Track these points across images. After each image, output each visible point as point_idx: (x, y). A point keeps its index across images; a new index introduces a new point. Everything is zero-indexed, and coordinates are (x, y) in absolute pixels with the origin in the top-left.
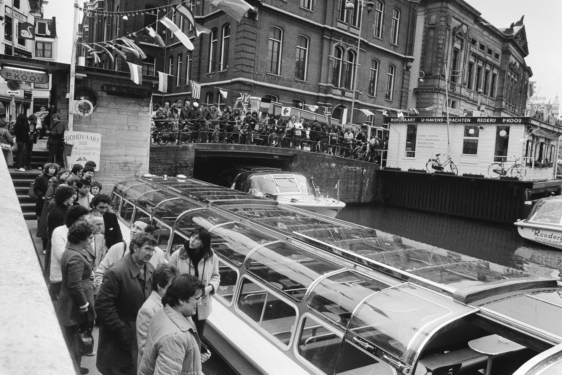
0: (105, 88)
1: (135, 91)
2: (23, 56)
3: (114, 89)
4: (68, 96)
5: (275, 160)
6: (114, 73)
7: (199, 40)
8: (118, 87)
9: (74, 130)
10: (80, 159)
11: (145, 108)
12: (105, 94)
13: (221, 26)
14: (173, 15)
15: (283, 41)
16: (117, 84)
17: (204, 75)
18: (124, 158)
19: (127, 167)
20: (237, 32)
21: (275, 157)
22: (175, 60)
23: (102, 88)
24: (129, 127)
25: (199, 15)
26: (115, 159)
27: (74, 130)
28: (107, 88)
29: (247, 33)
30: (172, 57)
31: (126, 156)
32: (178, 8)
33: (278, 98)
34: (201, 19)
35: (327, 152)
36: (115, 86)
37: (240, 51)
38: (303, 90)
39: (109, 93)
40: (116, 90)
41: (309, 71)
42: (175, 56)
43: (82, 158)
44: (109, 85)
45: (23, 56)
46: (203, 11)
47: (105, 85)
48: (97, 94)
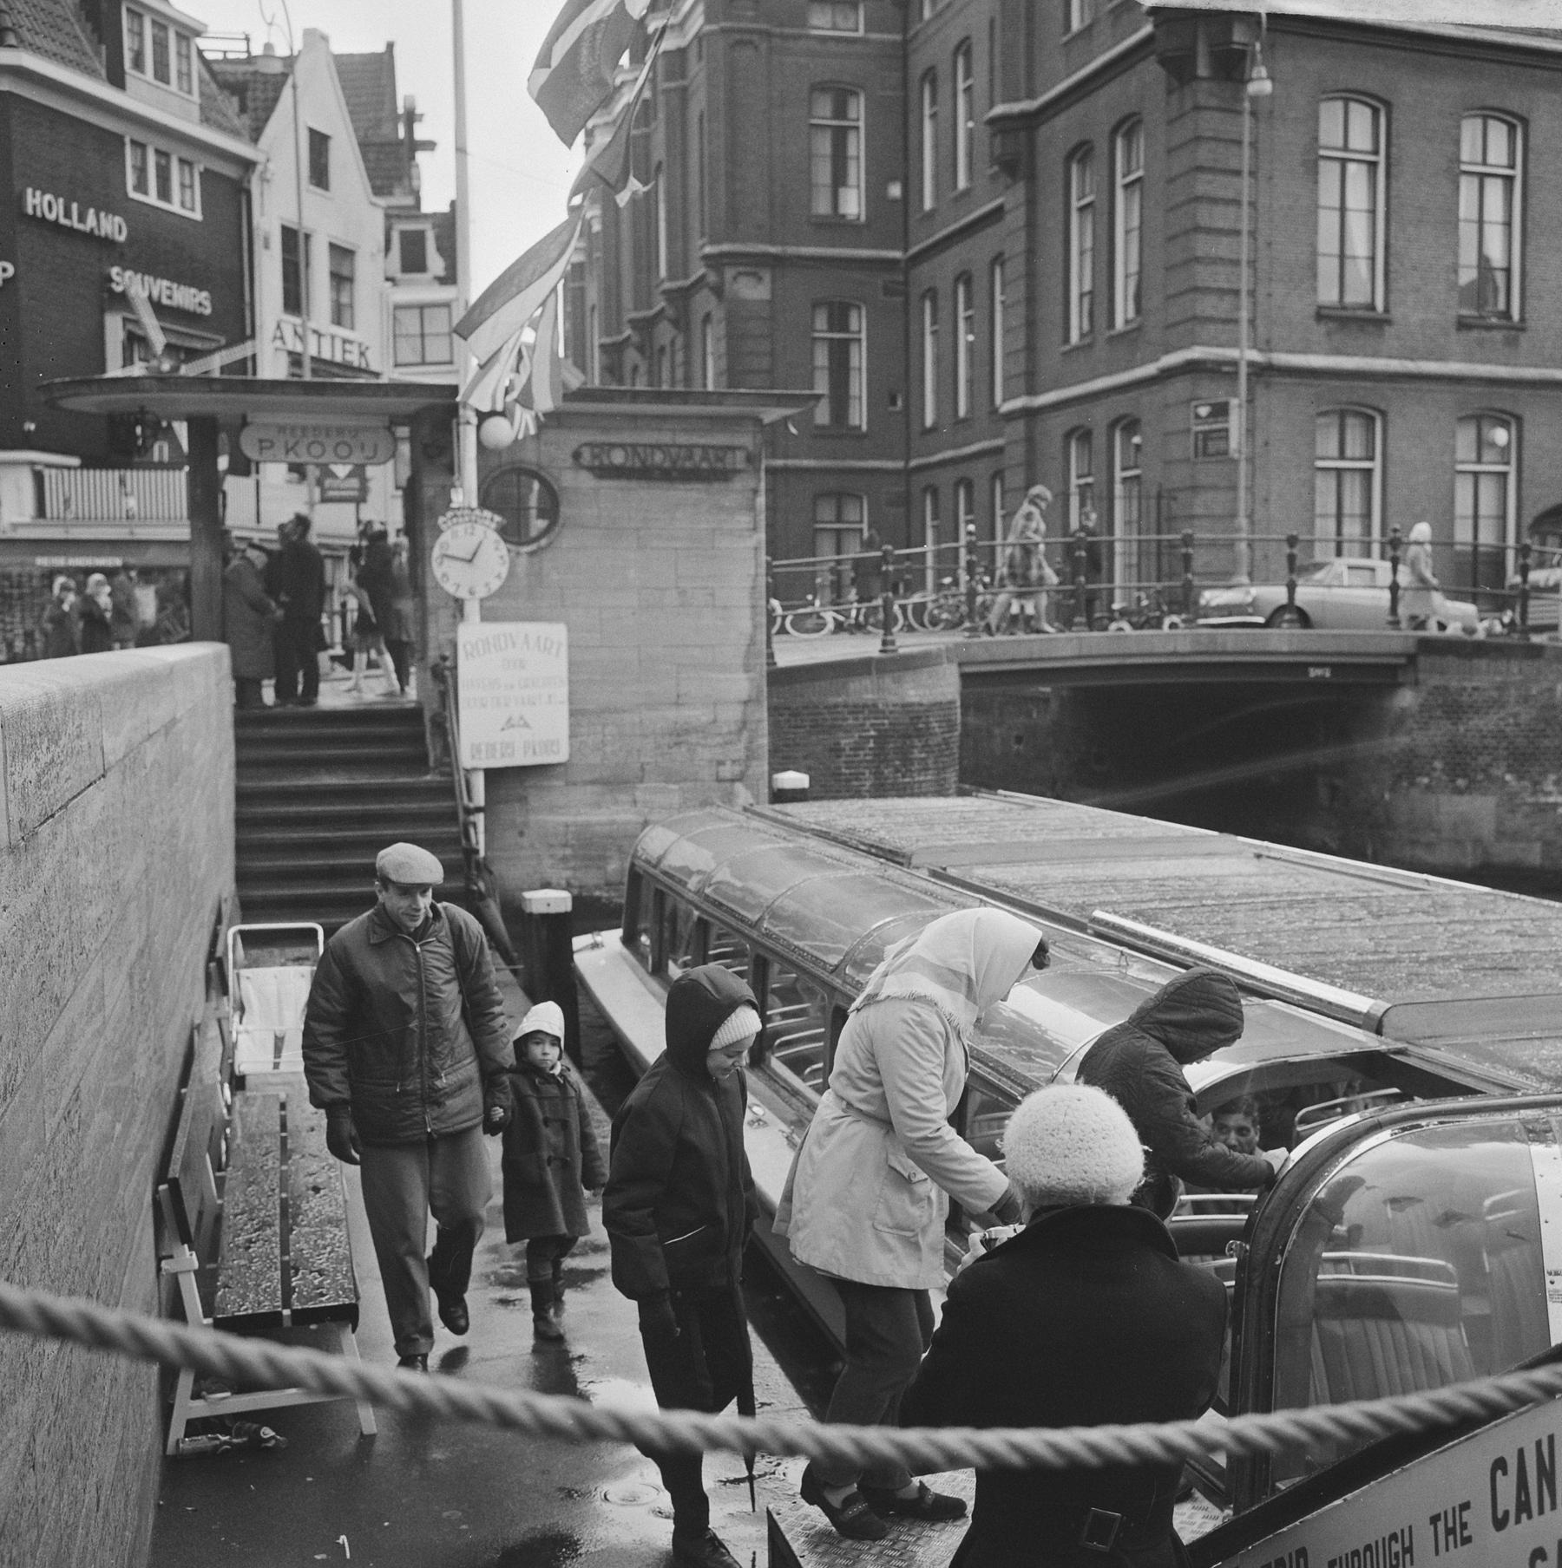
0: (586, 455)
1: (698, 453)
2: (666, 935)
3: (618, 457)
4: (1418, 1100)
5: (1319, 684)
6: (706, 398)
7: (1023, 210)
8: (634, 446)
9: (484, 619)
10: (509, 724)
11: (738, 518)
12: (586, 480)
13: (1107, 128)
14: (961, 86)
15: (1388, 157)
16: (627, 437)
17: (1050, 358)
18: (672, 714)
19: (684, 749)
20: (1170, 151)
21: (1314, 673)
22: (944, 303)
23: (577, 455)
24: (682, 593)
25: (1017, 100)
26: (637, 720)
27: (484, 619)
28: (594, 457)
29: (1213, 145)
30: (932, 293)
31: (677, 704)
32: (170, 521)
33: (1383, 414)
34: (1023, 115)
35: (970, 533)
36: (622, 446)
37: (1186, 232)
38: (1506, 364)
39: (606, 472)
40: (627, 458)
41: (1534, 273)
42: (944, 286)
43: (515, 721)
44: (601, 445)
45: (666, 935)
46: (1030, 75)
47: (586, 444)
48: (557, 480)
